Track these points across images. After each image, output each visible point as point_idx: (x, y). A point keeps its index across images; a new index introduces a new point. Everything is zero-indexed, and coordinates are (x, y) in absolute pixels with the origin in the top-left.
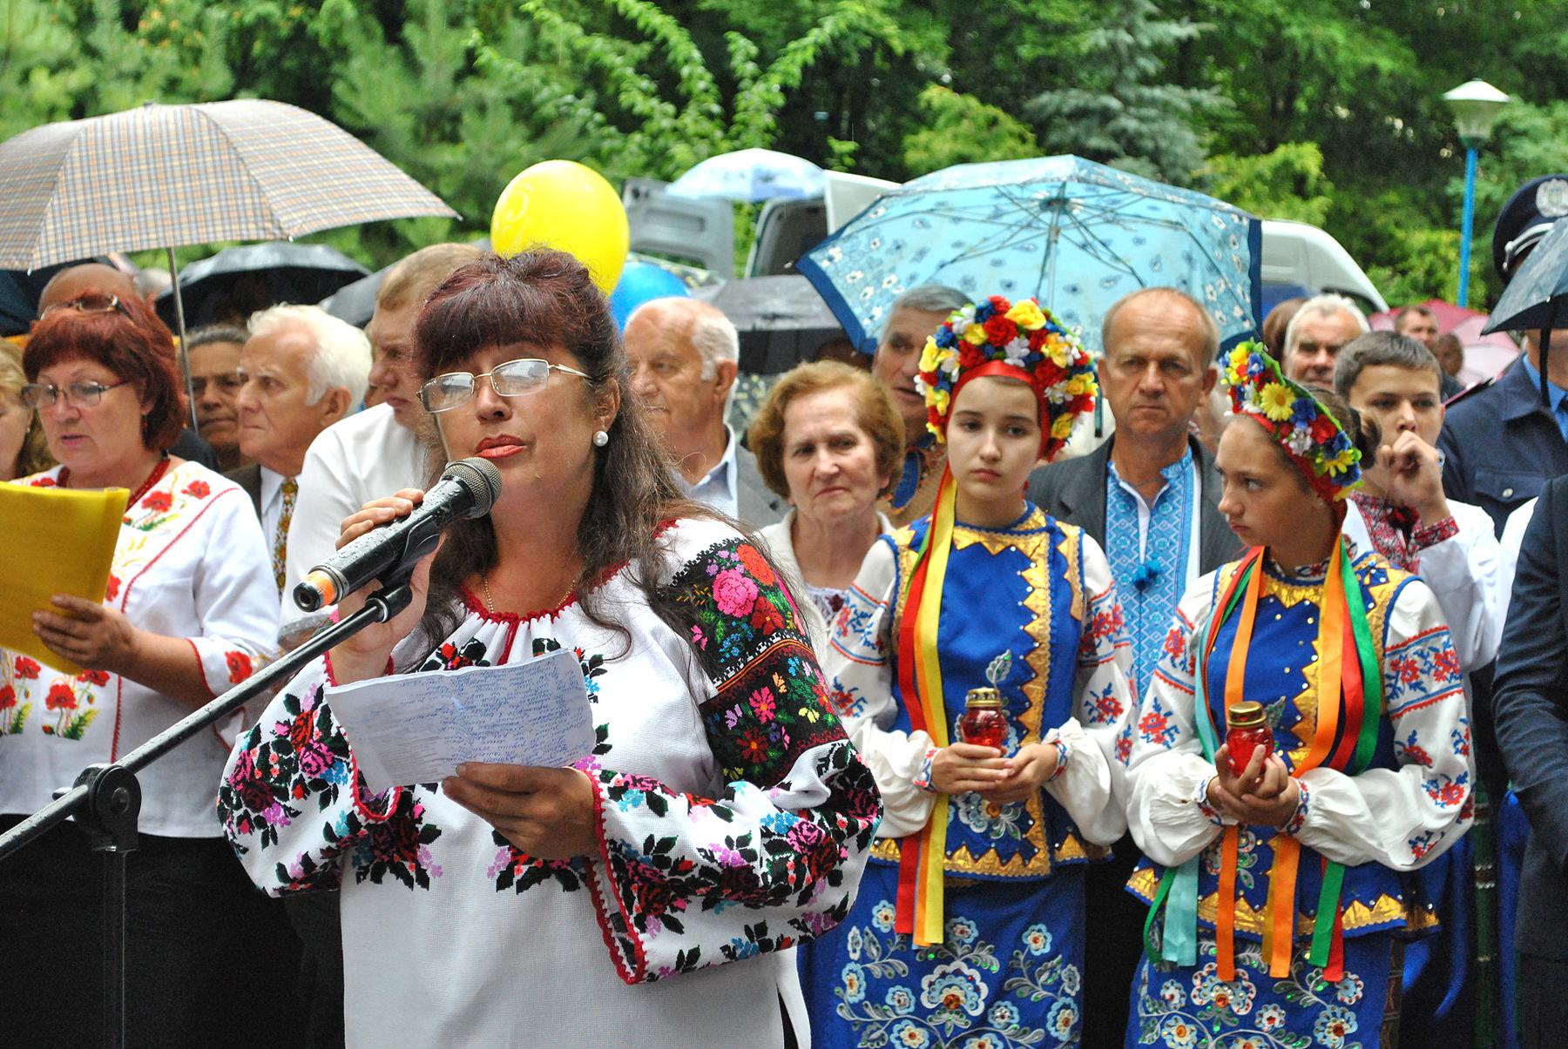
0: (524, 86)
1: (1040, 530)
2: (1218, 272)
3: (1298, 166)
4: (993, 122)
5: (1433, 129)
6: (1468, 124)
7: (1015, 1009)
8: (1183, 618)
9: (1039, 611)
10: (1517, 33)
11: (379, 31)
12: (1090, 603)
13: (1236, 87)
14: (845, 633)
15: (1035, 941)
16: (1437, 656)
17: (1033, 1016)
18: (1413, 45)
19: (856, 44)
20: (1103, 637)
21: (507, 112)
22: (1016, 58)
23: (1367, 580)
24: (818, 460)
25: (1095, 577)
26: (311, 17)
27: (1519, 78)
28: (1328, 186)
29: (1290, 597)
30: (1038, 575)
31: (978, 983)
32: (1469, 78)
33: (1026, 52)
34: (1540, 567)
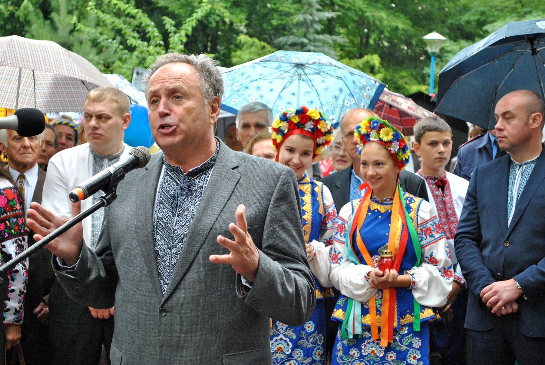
0: (93, 36)
1: (308, 183)
2: (353, 96)
3: (371, 63)
4: (264, 48)
5: (418, 50)
6: (431, 47)
7: (302, 351)
8: (342, 219)
9: (308, 211)
10: (447, 15)
11: (41, 15)
12: (325, 209)
13: (348, 35)
15: (309, 327)
16: (436, 226)
17: (308, 353)
18: (410, 19)
19: (214, 19)
20: (329, 220)
21: (90, 44)
22: (271, 25)
23: (408, 202)
25: (327, 200)
26: (16, 10)
27: (448, 31)
28: (382, 70)
29: (382, 209)
30: (307, 198)
31: (288, 342)
32: (430, 31)
33: (275, 22)
34: (472, 196)
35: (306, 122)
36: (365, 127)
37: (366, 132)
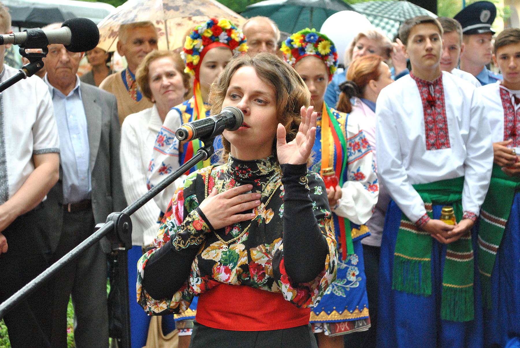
14: (163, 145)
24: (163, 81)
35: (219, 34)
36: (299, 40)
37: (300, 46)
